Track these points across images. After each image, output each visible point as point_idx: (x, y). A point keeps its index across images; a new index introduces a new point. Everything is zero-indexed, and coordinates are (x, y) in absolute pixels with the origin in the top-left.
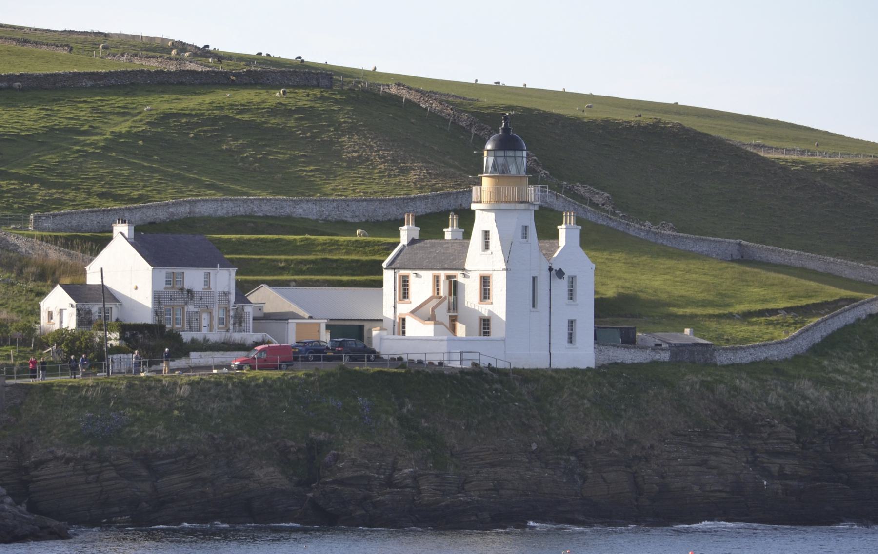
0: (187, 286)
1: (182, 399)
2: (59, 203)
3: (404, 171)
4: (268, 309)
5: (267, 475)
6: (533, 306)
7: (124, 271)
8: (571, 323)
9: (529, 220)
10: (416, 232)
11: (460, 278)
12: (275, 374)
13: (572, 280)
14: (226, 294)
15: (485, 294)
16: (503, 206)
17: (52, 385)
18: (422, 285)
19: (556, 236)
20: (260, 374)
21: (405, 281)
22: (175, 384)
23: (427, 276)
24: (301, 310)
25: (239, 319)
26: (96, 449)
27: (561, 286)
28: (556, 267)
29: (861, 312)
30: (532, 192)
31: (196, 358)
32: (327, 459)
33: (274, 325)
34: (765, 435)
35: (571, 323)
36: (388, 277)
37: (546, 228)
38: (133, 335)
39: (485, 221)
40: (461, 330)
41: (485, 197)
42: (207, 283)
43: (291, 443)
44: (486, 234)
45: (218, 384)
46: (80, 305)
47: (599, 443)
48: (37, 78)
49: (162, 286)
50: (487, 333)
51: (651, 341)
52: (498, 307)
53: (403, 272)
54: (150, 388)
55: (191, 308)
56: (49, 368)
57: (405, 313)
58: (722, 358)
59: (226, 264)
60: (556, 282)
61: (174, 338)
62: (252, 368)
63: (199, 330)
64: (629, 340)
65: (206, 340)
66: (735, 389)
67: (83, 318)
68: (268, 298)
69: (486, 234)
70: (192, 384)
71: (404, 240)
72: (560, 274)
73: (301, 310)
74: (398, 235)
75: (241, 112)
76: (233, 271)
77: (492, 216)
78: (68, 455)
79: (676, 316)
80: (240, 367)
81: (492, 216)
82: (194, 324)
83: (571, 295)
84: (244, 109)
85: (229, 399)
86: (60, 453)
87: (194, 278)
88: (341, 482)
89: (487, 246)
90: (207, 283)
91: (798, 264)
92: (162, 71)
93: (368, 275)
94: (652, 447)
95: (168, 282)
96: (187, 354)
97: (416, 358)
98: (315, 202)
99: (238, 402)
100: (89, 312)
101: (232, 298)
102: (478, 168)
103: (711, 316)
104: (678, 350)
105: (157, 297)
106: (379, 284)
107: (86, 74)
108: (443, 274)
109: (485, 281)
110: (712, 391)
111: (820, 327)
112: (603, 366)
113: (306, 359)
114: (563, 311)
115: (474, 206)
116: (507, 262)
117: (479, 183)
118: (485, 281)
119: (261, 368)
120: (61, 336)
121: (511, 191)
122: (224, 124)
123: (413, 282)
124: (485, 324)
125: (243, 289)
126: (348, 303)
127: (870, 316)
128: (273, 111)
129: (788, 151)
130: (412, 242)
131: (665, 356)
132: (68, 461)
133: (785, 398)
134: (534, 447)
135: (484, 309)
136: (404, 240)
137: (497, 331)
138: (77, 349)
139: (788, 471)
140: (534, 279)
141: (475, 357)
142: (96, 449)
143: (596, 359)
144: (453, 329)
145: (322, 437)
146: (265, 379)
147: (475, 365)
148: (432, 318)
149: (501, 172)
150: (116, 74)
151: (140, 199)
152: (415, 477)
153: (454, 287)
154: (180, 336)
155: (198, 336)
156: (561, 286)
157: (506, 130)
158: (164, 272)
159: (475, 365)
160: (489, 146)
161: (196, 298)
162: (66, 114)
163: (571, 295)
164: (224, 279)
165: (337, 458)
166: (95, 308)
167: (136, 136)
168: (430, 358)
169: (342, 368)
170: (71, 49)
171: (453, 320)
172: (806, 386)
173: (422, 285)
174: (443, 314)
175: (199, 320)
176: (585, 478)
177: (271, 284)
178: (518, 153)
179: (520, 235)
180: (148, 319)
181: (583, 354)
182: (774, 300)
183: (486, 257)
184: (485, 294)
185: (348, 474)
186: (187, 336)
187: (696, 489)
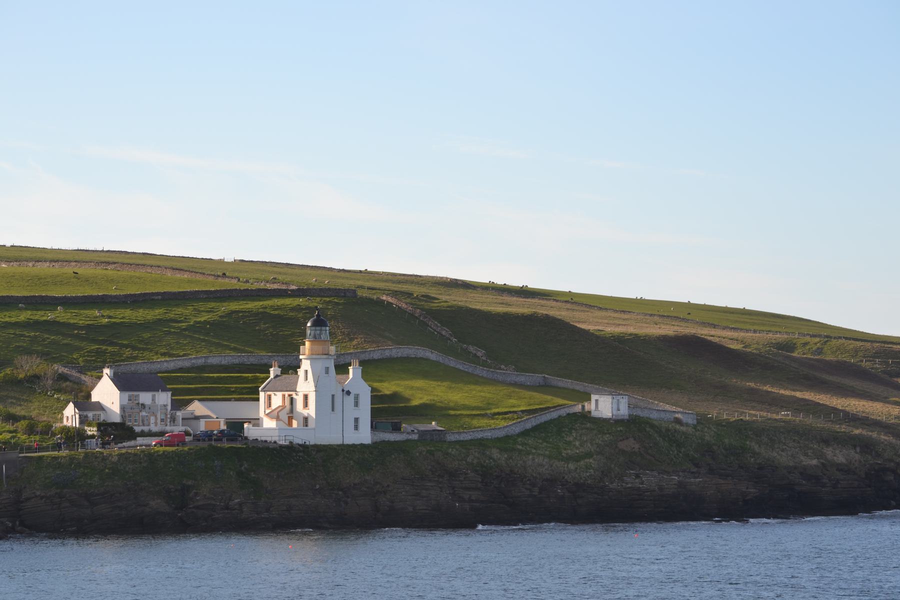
0: (141, 402)
1: (113, 463)
2: (136, 358)
3: (351, 340)
4: (198, 413)
5: (157, 504)
6: (333, 410)
7: (106, 393)
8: (356, 420)
9: (331, 365)
10: (279, 371)
11: (294, 396)
12: (174, 449)
13: (357, 397)
14: (165, 406)
15: (306, 405)
16: (314, 356)
17: (43, 456)
18: (277, 400)
19: (348, 373)
20: (162, 449)
21: (270, 397)
22: (111, 455)
23: (280, 394)
24: (209, 414)
25: (173, 420)
26: (58, 491)
27: (350, 400)
28: (346, 389)
29: (563, 412)
30: (332, 349)
31: (140, 440)
32: (191, 495)
33: (194, 422)
34: (462, 479)
35: (356, 420)
36: (262, 395)
37: (342, 369)
38: (105, 429)
39: (306, 365)
40: (295, 424)
41: (307, 352)
42: (153, 400)
43: (171, 486)
44: (306, 371)
45: (135, 455)
46: (81, 413)
47: (355, 484)
48: (174, 293)
49: (126, 402)
50: (307, 426)
51: (410, 428)
52: (311, 411)
53: (269, 393)
54: (96, 457)
55: (144, 413)
56: (57, 447)
57: (267, 417)
58: (451, 438)
59: (164, 390)
60: (346, 398)
61: (131, 429)
62: (161, 446)
63: (149, 425)
64: (396, 428)
65: (150, 431)
66: (447, 454)
67: (83, 420)
68: (197, 408)
69: (306, 371)
70: (121, 455)
71: (272, 376)
72: (348, 393)
73: (209, 414)
74: (269, 372)
75: (276, 310)
76: (170, 394)
77: (309, 362)
78: (43, 494)
79: (449, 415)
80: (155, 445)
81: (309, 362)
82: (146, 422)
83: (356, 404)
84: (279, 308)
85: (141, 463)
86: (38, 493)
87: (145, 397)
88: (197, 507)
89: (306, 379)
90: (153, 400)
91: (571, 387)
92: (247, 290)
93: (252, 395)
94: (388, 486)
95: (130, 400)
96: (135, 439)
97: (264, 439)
98: (282, 356)
99: (145, 465)
100: (87, 416)
101: (169, 408)
102: (303, 335)
103: (468, 416)
104: (423, 434)
105: (123, 408)
106: (258, 400)
107: (202, 291)
108: (287, 393)
109: (306, 397)
110: (433, 455)
111: (532, 422)
112: (376, 443)
113: (204, 440)
114: (351, 413)
115: (301, 357)
116: (316, 387)
117: (304, 344)
118: (306, 397)
119: (166, 446)
120: (66, 430)
121: (319, 348)
122: (262, 316)
123: (273, 397)
124: (306, 419)
125: (178, 405)
126: (236, 409)
127: (568, 414)
128: (293, 309)
129: (747, 331)
130: (276, 376)
131: (415, 437)
132: (42, 498)
133: (478, 458)
134: (318, 487)
135: (305, 412)
136: (272, 376)
137: (312, 424)
138: (74, 437)
139: (473, 498)
140: (333, 396)
141: (291, 438)
142: (58, 491)
143: (372, 439)
144: (290, 424)
145: (190, 483)
146: (164, 452)
147: (291, 442)
148: (278, 418)
149: (316, 339)
150: (220, 291)
151: (184, 355)
152: (240, 504)
153: (292, 400)
154: (132, 428)
155: (146, 429)
156: (350, 400)
157: (318, 316)
158: (127, 394)
159: (291, 442)
160: (309, 325)
161: (147, 408)
162: (177, 312)
163: (356, 404)
164: (164, 398)
165: (196, 494)
166: (90, 415)
167: (209, 323)
168: (269, 439)
169: (211, 445)
170: (239, 280)
171: (290, 419)
172: (495, 453)
173: (277, 400)
174: (284, 416)
175: (149, 420)
176: (346, 503)
177: (200, 400)
178: (323, 328)
179: (324, 371)
180: (117, 419)
181: (364, 436)
182: (519, 406)
183: (306, 384)
184: (306, 405)
185: (200, 503)
186: (137, 429)
187: (411, 509)
